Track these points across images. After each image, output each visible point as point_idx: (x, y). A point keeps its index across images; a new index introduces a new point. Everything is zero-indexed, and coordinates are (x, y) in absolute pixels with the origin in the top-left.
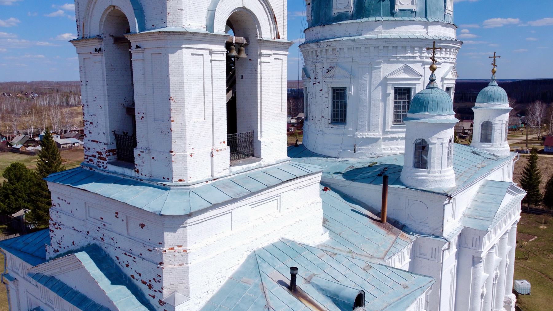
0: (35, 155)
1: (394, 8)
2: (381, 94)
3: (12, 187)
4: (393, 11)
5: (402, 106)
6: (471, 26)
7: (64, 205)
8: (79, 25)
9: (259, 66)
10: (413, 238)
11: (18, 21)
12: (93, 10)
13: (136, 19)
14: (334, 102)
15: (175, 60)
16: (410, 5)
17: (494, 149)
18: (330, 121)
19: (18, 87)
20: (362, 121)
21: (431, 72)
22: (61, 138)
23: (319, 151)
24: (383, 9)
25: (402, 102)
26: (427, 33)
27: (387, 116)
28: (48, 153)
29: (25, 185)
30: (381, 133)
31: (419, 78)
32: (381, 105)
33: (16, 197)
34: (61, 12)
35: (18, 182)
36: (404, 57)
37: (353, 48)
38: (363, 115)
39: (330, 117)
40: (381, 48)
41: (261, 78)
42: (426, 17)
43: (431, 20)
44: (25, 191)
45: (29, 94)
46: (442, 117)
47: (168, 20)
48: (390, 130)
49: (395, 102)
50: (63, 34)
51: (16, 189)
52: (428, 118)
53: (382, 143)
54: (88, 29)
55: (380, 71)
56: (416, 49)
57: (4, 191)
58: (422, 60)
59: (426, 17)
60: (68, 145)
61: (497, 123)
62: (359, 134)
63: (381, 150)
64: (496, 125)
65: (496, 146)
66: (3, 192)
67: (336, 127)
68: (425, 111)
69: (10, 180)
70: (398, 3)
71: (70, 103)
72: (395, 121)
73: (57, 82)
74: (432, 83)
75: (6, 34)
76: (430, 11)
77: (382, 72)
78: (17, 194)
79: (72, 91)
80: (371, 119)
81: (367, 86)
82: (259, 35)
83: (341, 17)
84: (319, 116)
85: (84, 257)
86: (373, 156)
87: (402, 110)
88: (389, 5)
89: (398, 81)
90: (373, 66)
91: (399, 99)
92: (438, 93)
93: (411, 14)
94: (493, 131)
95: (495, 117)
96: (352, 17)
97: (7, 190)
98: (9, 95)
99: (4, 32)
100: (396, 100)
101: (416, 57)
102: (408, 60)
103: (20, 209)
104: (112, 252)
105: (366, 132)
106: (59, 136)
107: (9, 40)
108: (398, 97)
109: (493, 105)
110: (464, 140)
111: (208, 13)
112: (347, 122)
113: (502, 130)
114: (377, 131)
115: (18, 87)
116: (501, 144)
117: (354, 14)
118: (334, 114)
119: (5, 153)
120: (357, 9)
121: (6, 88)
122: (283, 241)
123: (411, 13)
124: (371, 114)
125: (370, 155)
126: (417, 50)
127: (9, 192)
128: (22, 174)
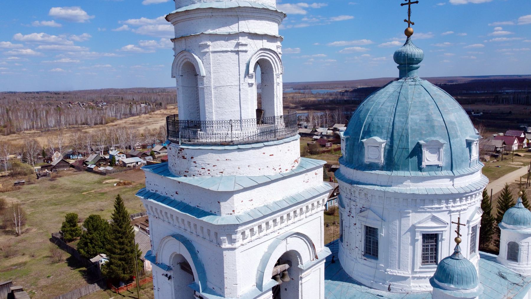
0: (105, 175)
1: (421, 164)
2: (410, 238)
3: (90, 236)
4: (421, 167)
5: (430, 248)
6: (505, 23)
8: (152, 245)
9: (300, 286)
11: (90, 36)
12: (164, 246)
13: (199, 282)
14: (367, 237)
15: (229, 266)
16: (437, 161)
17: (520, 269)
18: (363, 253)
19: (90, 96)
20: (392, 260)
21: (456, 244)
22: (127, 158)
23: (355, 276)
24: (411, 164)
25: (430, 245)
26: (453, 185)
27: (415, 258)
28: (120, 217)
29: (100, 234)
30: (410, 272)
31: (446, 226)
32: (410, 248)
33: (94, 245)
34: (125, 27)
35: (95, 231)
36: (432, 208)
37: (383, 197)
38: (394, 255)
39: (363, 250)
40: (410, 200)
41: (302, 296)
42: (452, 170)
43: (456, 174)
44: (100, 239)
45: (99, 103)
46: (467, 290)
47: (226, 292)
48: (418, 270)
49: (423, 246)
50: (126, 45)
52: (453, 291)
53: (412, 281)
54: (160, 258)
55: (409, 220)
56: (442, 201)
57: (84, 239)
58: (449, 209)
59: (452, 170)
60: (133, 164)
61: (523, 245)
62: (391, 271)
63: (410, 287)
64: (522, 247)
65: (523, 266)
66: (83, 240)
67: (369, 260)
68: (450, 283)
69: (88, 230)
70: (425, 160)
71: (133, 112)
72: (423, 262)
73: (122, 89)
74: (457, 254)
75: (79, 47)
76: (456, 164)
77: (410, 220)
78: (94, 243)
79: (135, 99)
80: (401, 260)
81: (397, 231)
82: (300, 263)
83: (372, 167)
84: (353, 246)
86: (403, 291)
87: (430, 252)
88: (417, 161)
89: (425, 229)
90: (402, 215)
91: (427, 243)
92: (463, 266)
93: (437, 169)
94: (519, 252)
95: (521, 240)
96: (382, 168)
97: (86, 238)
98: (83, 104)
99: (78, 46)
100: (425, 243)
101: (442, 207)
102: (435, 210)
103: (97, 255)
105: (396, 269)
106: (125, 155)
107: (83, 53)
108: (426, 241)
109: (520, 229)
110: (495, 160)
111: (258, 272)
112: (379, 258)
113: (528, 251)
114: (407, 270)
115: (90, 96)
116: (527, 264)
117: (385, 166)
118: (367, 247)
119: (81, 172)
120: (387, 161)
123: (438, 168)
124: (401, 255)
125: (400, 291)
126: (443, 202)
127: (88, 241)
128: (98, 225)
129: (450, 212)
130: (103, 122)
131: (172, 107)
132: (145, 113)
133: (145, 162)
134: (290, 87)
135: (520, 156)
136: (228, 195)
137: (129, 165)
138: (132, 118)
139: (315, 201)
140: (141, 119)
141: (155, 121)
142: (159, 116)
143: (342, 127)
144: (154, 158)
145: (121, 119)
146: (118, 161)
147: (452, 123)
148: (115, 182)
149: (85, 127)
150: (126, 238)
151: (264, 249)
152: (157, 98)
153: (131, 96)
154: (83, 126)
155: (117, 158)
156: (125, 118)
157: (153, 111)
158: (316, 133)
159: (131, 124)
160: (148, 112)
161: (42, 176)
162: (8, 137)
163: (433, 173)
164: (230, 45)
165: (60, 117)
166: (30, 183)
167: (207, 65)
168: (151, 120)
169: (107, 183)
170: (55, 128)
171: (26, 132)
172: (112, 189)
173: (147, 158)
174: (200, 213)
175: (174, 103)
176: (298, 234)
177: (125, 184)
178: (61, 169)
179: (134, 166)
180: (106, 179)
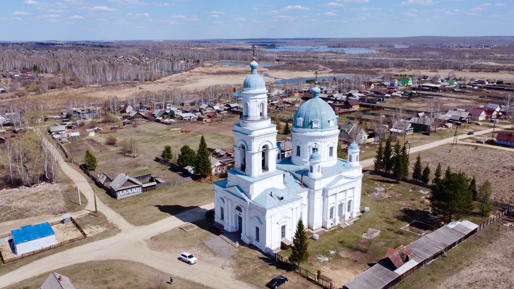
3: (185, 156)
7: (231, 177)
10: (308, 189)
51: (186, 157)
60: (188, 118)
62: (303, 160)
83: (299, 127)
85: (235, 187)
90: (307, 142)
98: (128, 59)
104: (241, 187)
121: (124, 52)
122: (272, 188)
129: (321, 142)
130: (152, 79)
131: (209, 64)
132: (186, 71)
133: (197, 117)
134: (325, 43)
135: (479, 125)
136: (253, 131)
137: (185, 118)
138: (174, 76)
139: (273, 134)
140: (183, 76)
141: (195, 79)
142: (198, 74)
143: (356, 93)
144: (202, 114)
145: (166, 76)
146: (177, 115)
147: (324, 115)
148: (179, 130)
149: (136, 83)
150: (206, 155)
151: (260, 143)
153: (170, 51)
154: (136, 82)
155: (176, 113)
156: (169, 75)
157: (193, 69)
158: (332, 98)
159: (175, 81)
160: (188, 70)
161: (127, 124)
163: (316, 130)
164: (255, 100)
165: (116, 74)
167: (250, 104)
168: (191, 78)
169: (173, 131)
170: (113, 83)
171: (90, 85)
172: (178, 135)
173: (197, 114)
174: (247, 134)
176: (268, 141)
177: (186, 132)
178: (137, 119)
179: (189, 120)
180: (171, 128)
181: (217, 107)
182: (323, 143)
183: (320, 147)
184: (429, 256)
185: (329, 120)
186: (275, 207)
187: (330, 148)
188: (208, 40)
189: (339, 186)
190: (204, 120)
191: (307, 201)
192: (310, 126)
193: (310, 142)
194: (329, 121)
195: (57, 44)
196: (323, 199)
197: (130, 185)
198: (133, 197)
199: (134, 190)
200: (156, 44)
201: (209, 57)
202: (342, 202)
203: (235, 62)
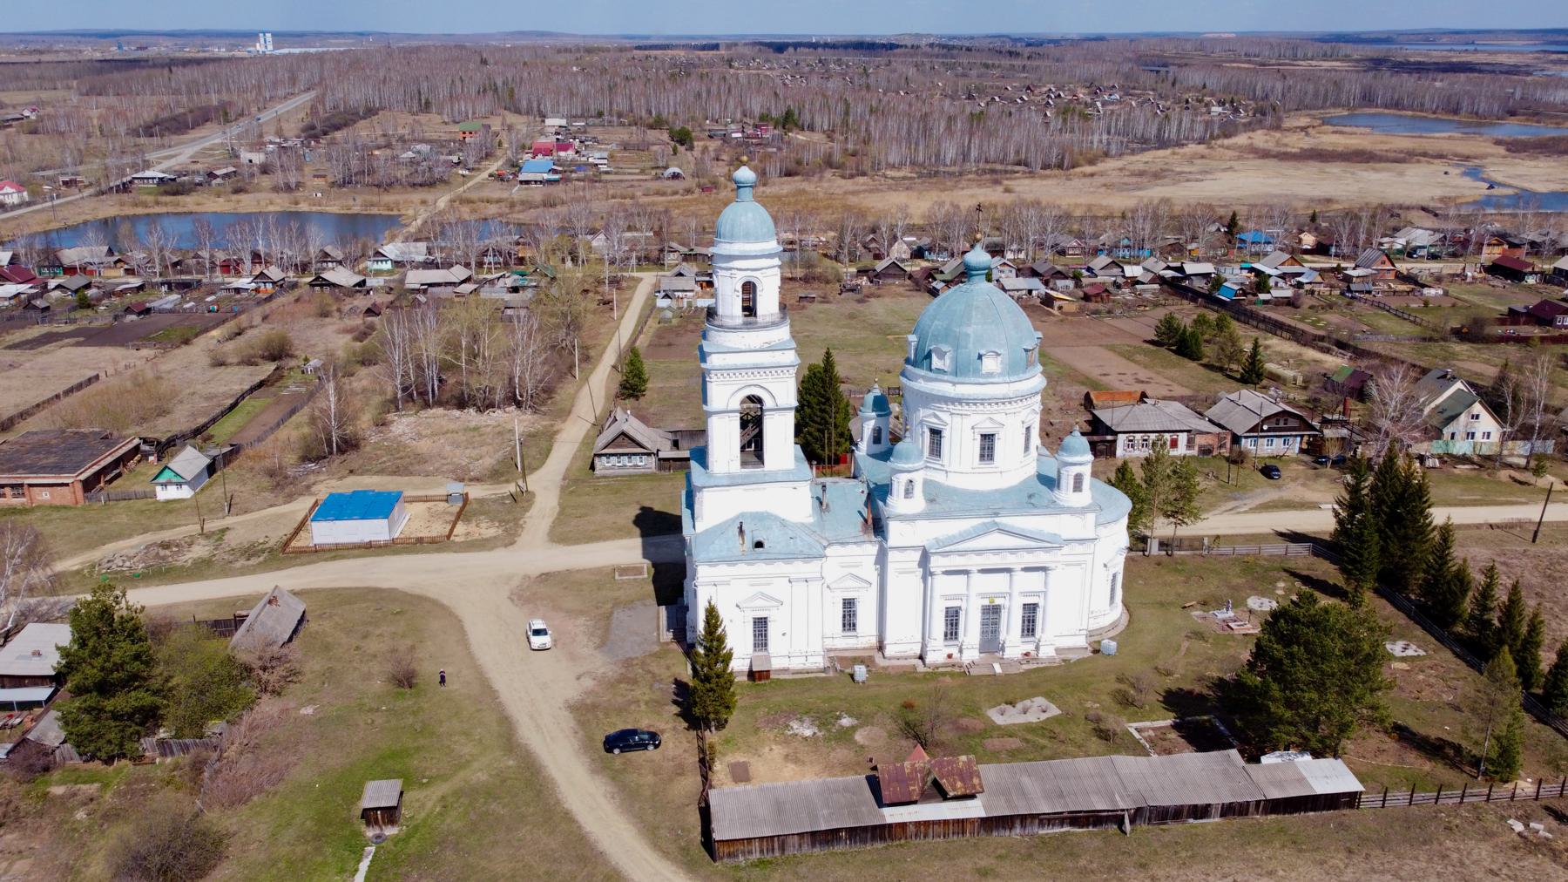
19: (1089, 69)
131: (1304, 121)
147: (968, 335)
152: (1273, 88)
159: (1133, 174)
162: (848, 185)
164: (728, 273)
166: (825, 300)
170: (952, 169)
175: (1322, 108)
178: (890, 281)
181: (1132, 271)
182: (957, 419)
183: (948, 427)
184: (1044, 808)
185: (982, 352)
186: (731, 561)
187: (984, 437)
188: (1389, 32)
189: (979, 552)
190: (1057, 304)
191: (876, 573)
192: (926, 362)
193: (924, 407)
194: (980, 357)
195: (906, 46)
196: (924, 579)
197: (626, 446)
198: (630, 476)
199: (636, 460)
200: (1189, 46)
201: (1321, 98)
202: (997, 602)
203: (1413, 117)
